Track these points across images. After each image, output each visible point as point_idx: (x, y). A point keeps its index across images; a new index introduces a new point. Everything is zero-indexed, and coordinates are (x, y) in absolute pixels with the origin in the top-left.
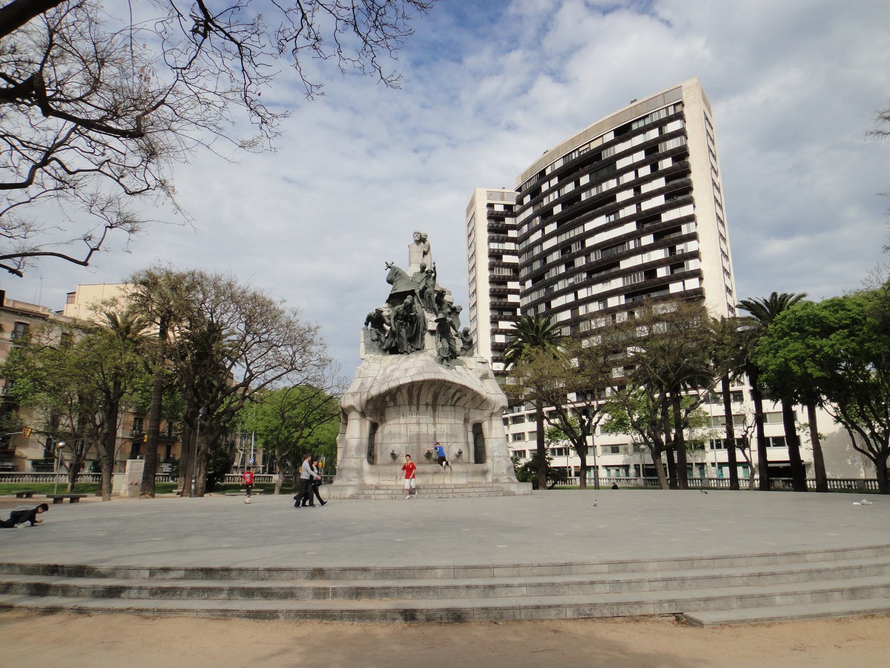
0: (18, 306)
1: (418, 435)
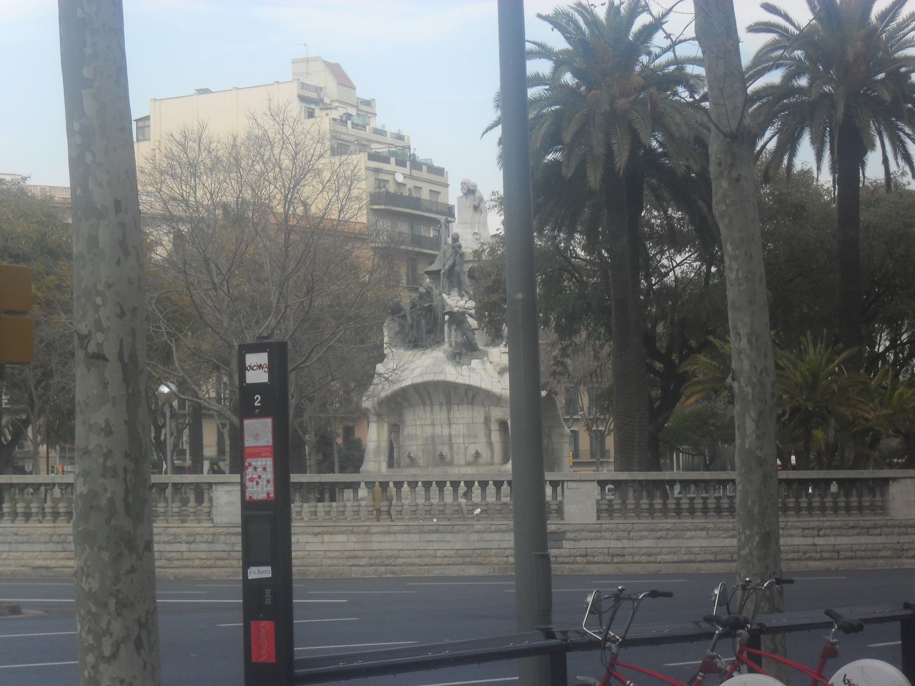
0: (443, 671)
1: (433, 437)
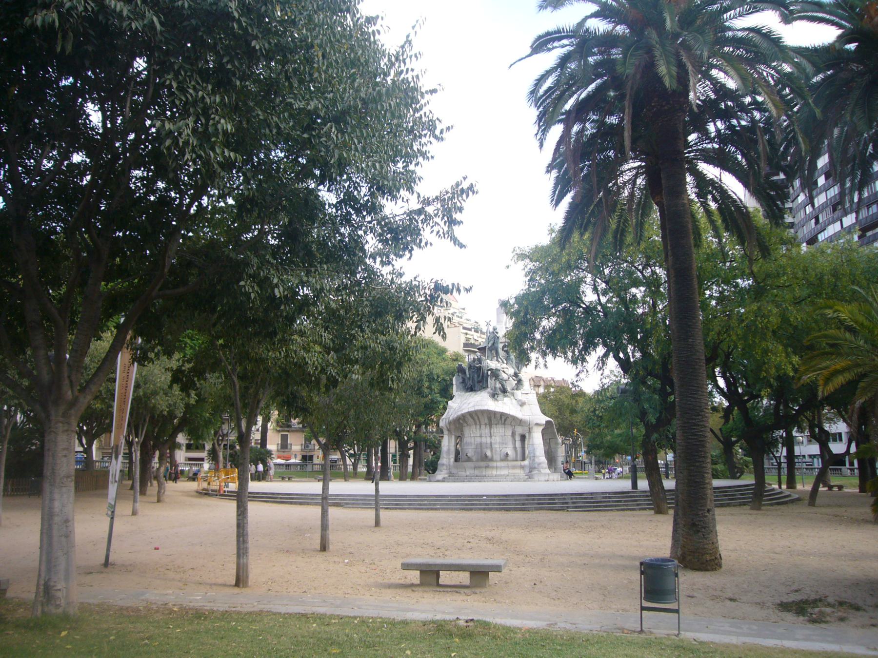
1: (481, 443)
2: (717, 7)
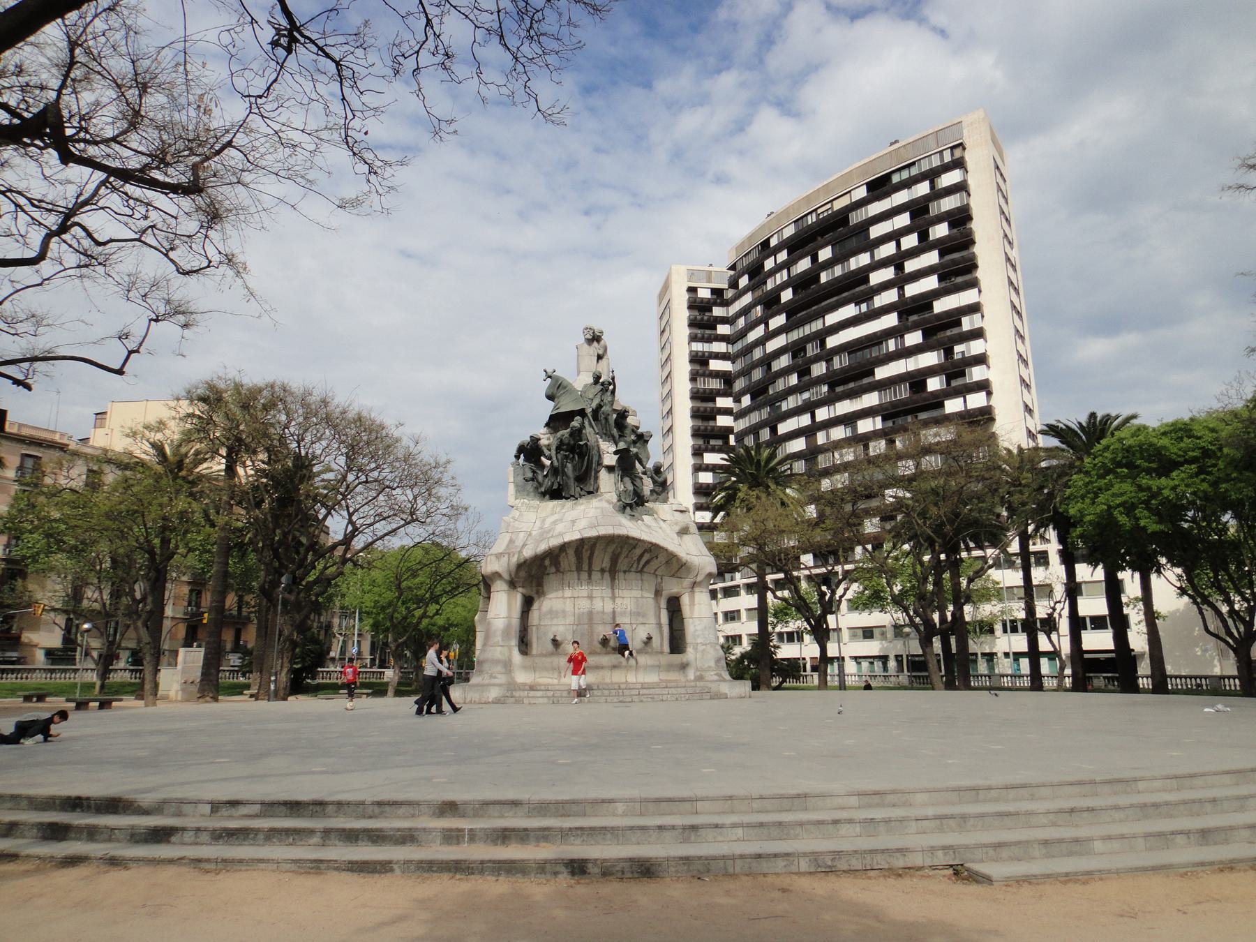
1: (591, 614)
2: (1121, 513)
